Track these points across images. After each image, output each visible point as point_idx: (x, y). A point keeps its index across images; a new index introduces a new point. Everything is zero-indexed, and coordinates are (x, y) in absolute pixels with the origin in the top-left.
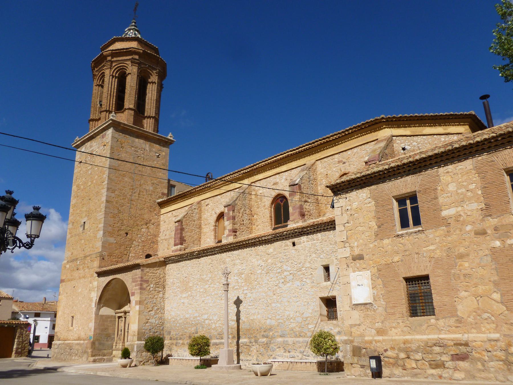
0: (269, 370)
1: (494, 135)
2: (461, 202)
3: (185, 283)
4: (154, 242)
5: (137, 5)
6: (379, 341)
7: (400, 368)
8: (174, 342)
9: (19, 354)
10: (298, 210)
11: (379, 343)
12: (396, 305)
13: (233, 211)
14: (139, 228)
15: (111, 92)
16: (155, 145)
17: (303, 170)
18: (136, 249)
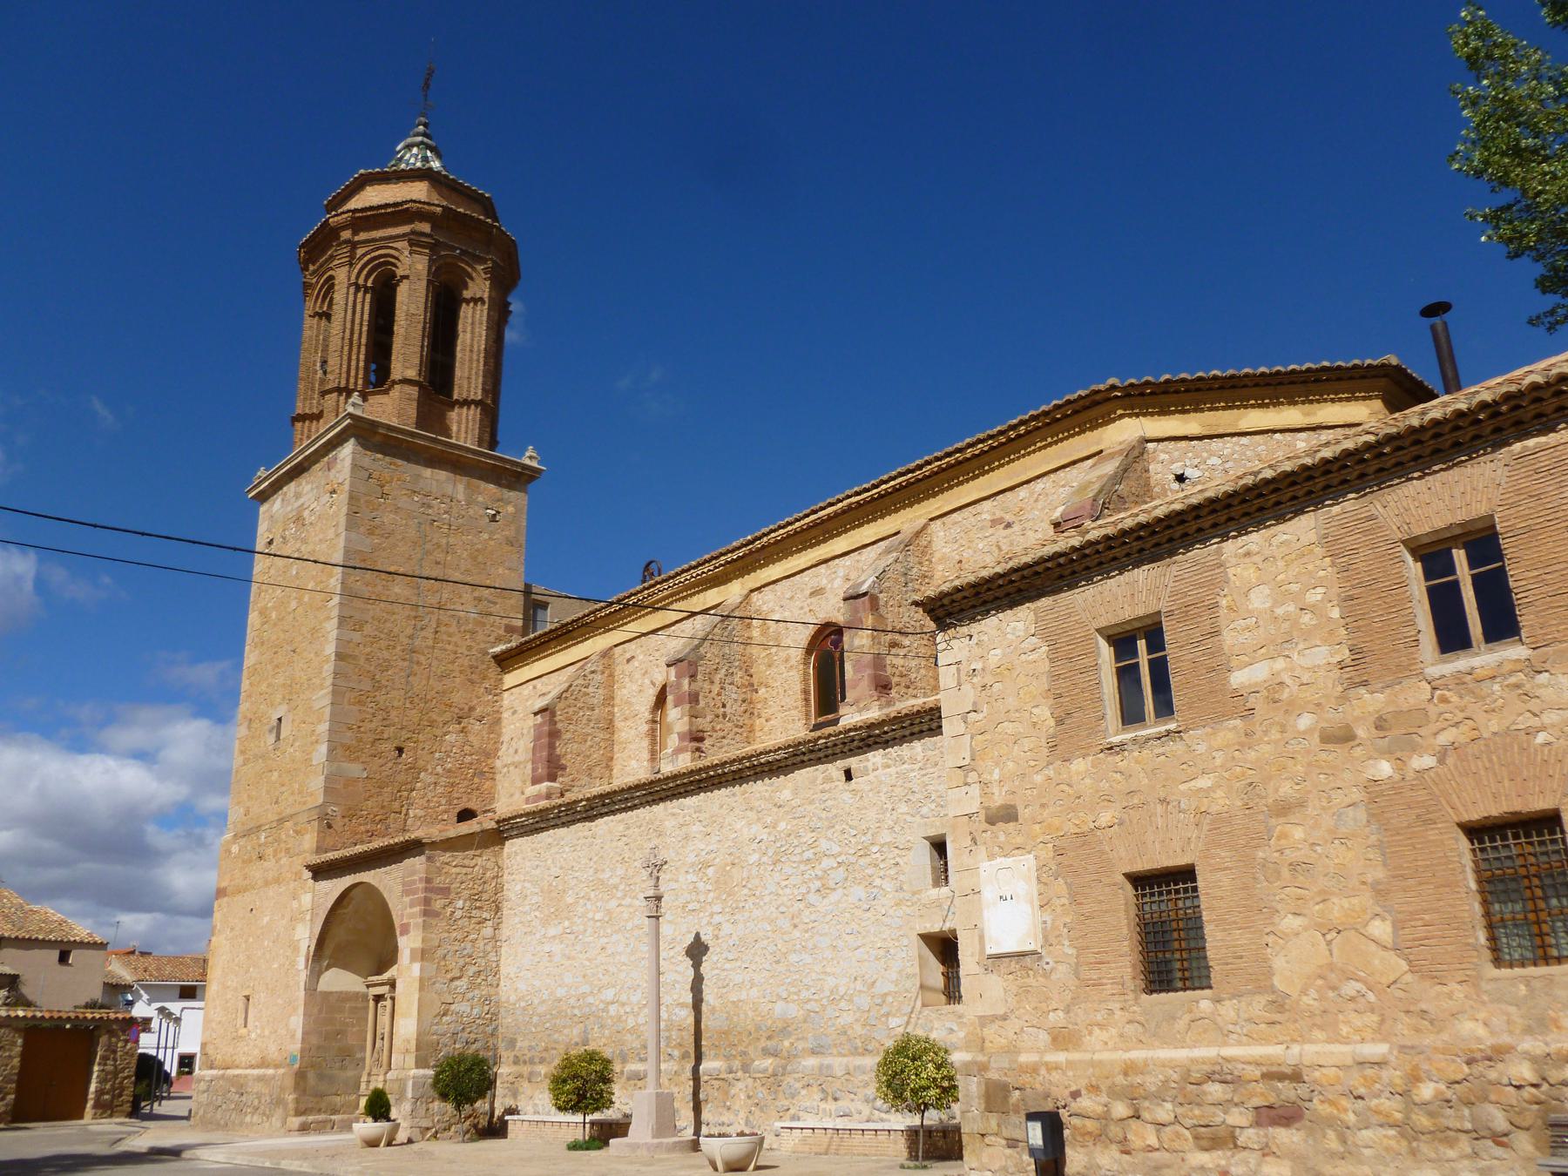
0: (749, 1156)
1: (1371, 438)
2: (1283, 644)
3: (554, 894)
4: (482, 773)
5: (431, 73)
6: (1057, 1067)
7: (1114, 1147)
8: (525, 1070)
9: (106, 1108)
10: (869, 671)
11: (1057, 1072)
12: (1105, 957)
13: (693, 676)
15: (352, 333)
16: (483, 484)
17: (888, 551)
18: (430, 795)
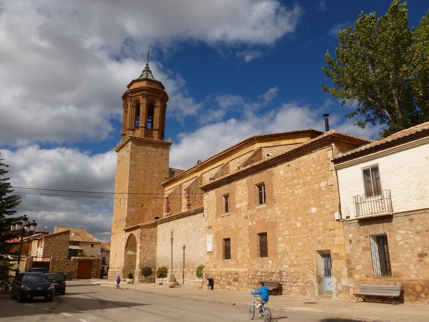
14: (150, 201)
